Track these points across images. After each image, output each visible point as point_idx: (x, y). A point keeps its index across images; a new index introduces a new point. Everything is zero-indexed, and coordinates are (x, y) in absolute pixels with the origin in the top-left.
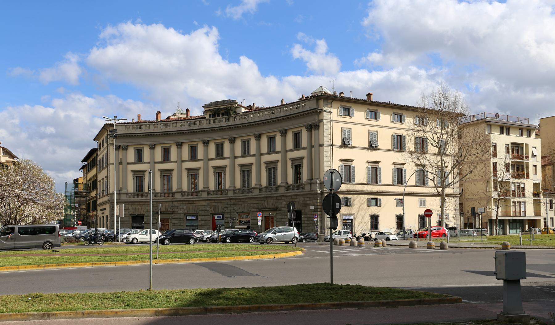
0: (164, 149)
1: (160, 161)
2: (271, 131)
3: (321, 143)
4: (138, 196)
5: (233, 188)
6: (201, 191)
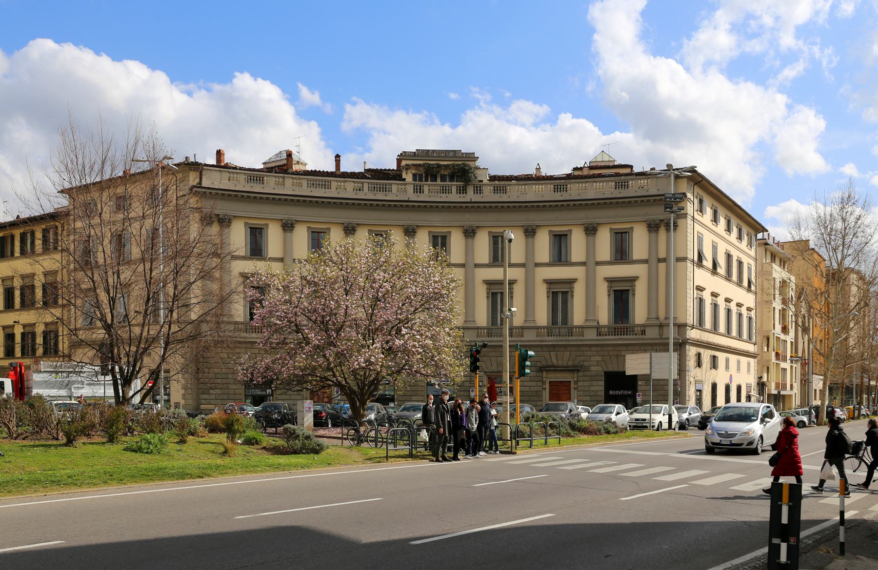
0: (434, 236)
1: (486, 261)
2: (623, 220)
3: (680, 255)
4: (615, 331)
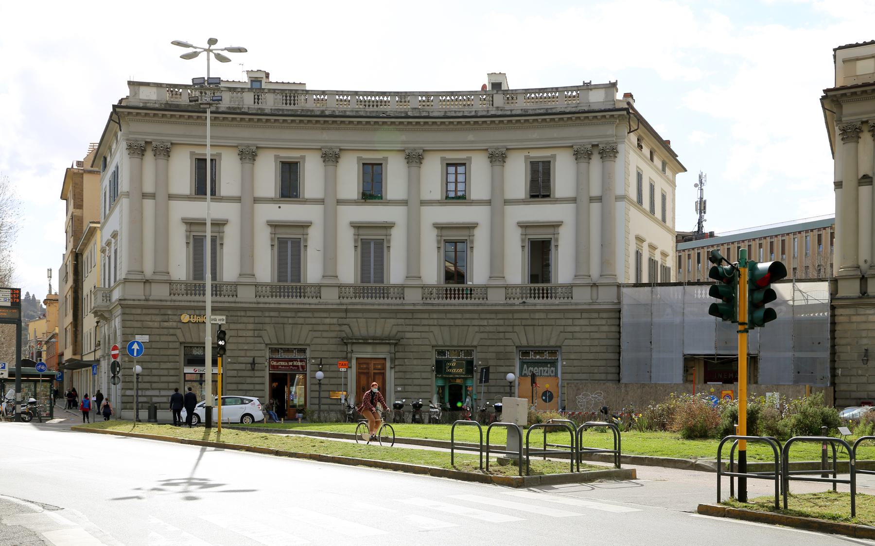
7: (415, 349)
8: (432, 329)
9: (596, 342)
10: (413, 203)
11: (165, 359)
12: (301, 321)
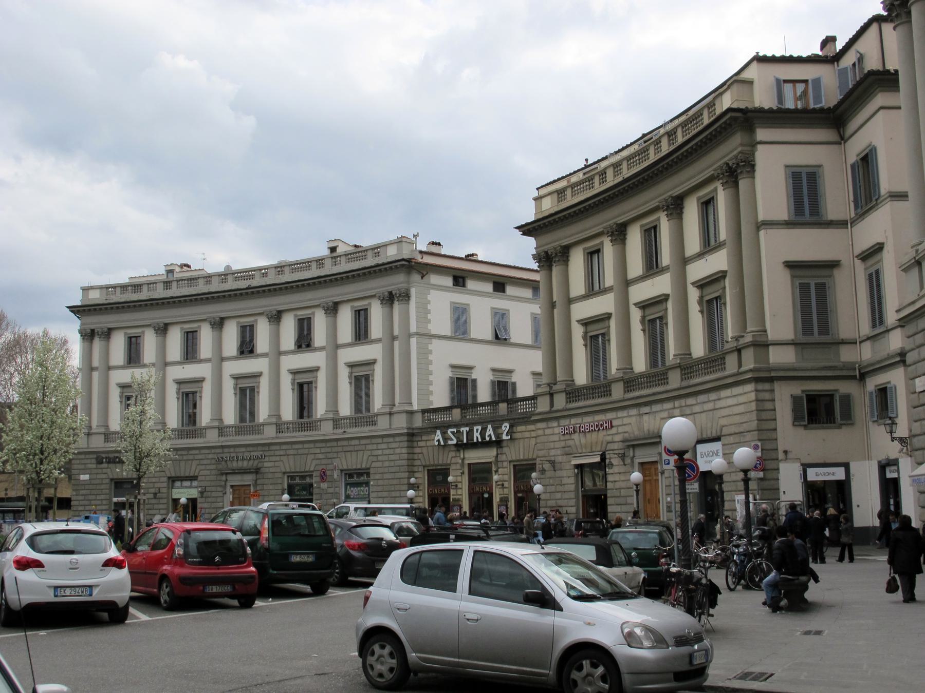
5: (274, 420)
6: (205, 428)
7: (270, 476)
8: (283, 458)
9: (392, 464)
10: (335, 346)
11: (99, 492)
12: (191, 457)
